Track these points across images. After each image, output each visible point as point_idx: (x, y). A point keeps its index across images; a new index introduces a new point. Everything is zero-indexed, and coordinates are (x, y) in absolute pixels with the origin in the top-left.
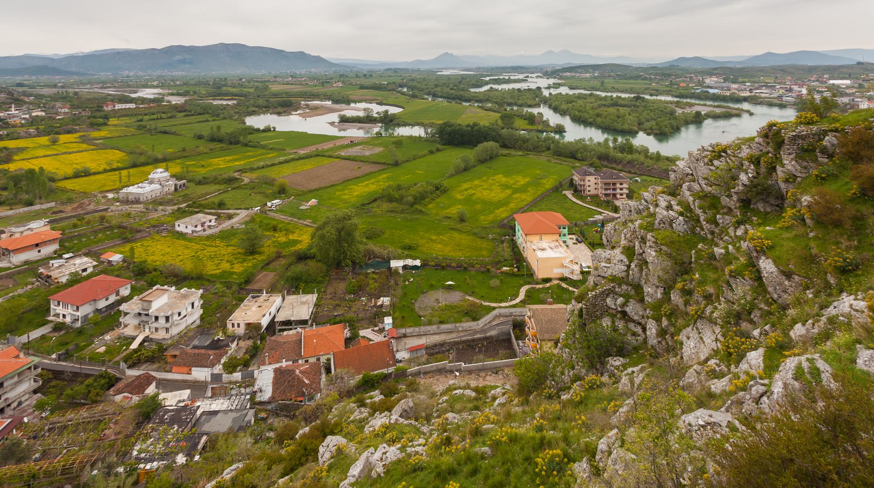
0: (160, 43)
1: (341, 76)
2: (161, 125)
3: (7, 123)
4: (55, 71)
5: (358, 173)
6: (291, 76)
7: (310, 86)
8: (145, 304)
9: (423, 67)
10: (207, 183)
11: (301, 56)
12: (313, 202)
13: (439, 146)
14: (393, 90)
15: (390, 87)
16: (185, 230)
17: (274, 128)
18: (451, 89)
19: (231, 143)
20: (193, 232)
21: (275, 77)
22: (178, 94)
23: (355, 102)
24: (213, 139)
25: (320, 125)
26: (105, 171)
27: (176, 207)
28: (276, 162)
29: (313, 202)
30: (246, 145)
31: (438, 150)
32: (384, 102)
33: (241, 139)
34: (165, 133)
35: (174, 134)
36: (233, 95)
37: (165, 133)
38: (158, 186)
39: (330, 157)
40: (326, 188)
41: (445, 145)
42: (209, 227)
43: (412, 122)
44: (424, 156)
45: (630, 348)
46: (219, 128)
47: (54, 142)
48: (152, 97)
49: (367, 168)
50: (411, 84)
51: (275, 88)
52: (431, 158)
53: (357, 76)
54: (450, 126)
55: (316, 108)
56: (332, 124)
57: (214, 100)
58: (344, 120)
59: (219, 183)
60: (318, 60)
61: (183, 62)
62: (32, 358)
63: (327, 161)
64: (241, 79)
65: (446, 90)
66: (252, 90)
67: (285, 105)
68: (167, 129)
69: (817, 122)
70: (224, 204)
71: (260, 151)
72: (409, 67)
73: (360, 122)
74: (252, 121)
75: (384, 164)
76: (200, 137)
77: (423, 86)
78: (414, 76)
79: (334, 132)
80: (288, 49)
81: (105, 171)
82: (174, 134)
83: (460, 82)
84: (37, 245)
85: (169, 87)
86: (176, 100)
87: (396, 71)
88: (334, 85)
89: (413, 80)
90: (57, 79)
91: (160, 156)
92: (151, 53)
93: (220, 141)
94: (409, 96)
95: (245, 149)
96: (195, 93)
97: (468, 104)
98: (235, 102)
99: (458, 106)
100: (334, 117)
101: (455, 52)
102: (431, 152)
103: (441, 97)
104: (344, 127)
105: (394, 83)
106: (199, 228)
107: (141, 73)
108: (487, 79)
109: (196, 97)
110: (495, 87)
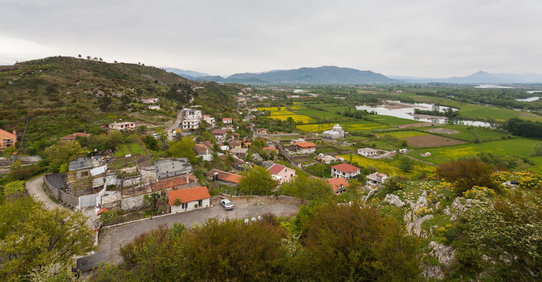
0: (297, 67)
2: (319, 106)
3: (258, 100)
5: (448, 143)
7: (381, 92)
8: (379, 178)
9: (460, 82)
10: (358, 135)
11: (369, 74)
12: (428, 154)
13: (511, 135)
14: (444, 97)
15: (440, 94)
16: (363, 154)
17: (376, 113)
19: (357, 118)
20: (368, 156)
21: (357, 86)
23: (418, 102)
24: (346, 115)
25: (404, 113)
26: (308, 124)
27: (352, 144)
29: (428, 154)
30: (366, 120)
31: (509, 138)
32: (441, 103)
33: (363, 116)
34: (321, 110)
35: (324, 111)
37: (321, 110)
38: (338, 133)
39: (422, 132)
40: (431, 148)
41: (514, 135)
42: (375, 155)
43: (474, 118)
44: (498, 140)
47: (279, 109)
49: (452, 142)
50: (456, 93)
51: (360, 92)
55: (393, 104)
56: (410, 114)
58: (418, 112)
59: (363, 136)
60: (380, 76)
61: (307, 76)
63: (421, 134)
64: (338, 86)
67: (374, 101)
68: (322, 108)
70: (375, 146)
71: (376, 124)
73: (429, 115)
74: (359, 108)
75: (466, 141)
76: (339, 114)
79: (411, 118)
80: (361, 70)
81: (308, 124)
82: (324, 111)
83: (504, 94)
84: (309, 147)
86: (315, 95)
87: (438, 84)
88: (408, 93)
90: (254, 84)
91: (328, 120)
92: (293, 71)
93: (351, 116)
94: (460, 101)
95: (366, 122)
97: (519, 110)
99: (511, 111)
100: (412, 111)
101: (490, 71)
102: (504, 138)
103: (488, 103)
104: (418, 116)
105: (443, 92)
106: (370, 154)
107: (289, 82)
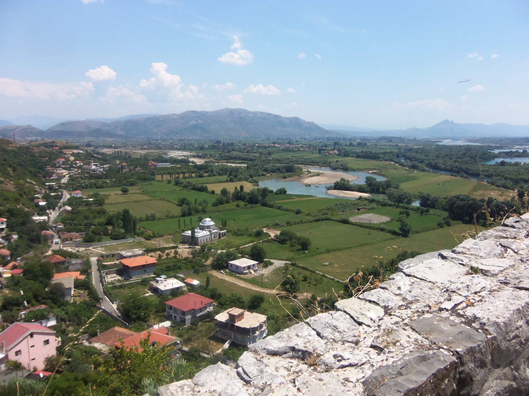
1: (336, 144)
4: (108, 134)
6: (289, 143)
9: (420, 137)
18: (455, 161)
21: (274, 143)
22: (199, 157)
28: (419, 280)
36: (243, 160)
45: (450, 312)
46: (242, 188)
48: (180, 158)
52: (440, 231)
53: (351, 145)
54: (462, 200)
57: (227, 162)
62: (174, 338)
65: (450, 162)
66: (258, 155)
67: (289, 170)
69: (35, 147)
72: (403, 135)
77: (423, 157)
78: (411, 145)
85: (190, 150)
86: (199, 162)
89: (410, 150)
96: (211, 156)
98: (245, 165)
108: (497, 151)
109: (212, 159)
110: (508, 160)
